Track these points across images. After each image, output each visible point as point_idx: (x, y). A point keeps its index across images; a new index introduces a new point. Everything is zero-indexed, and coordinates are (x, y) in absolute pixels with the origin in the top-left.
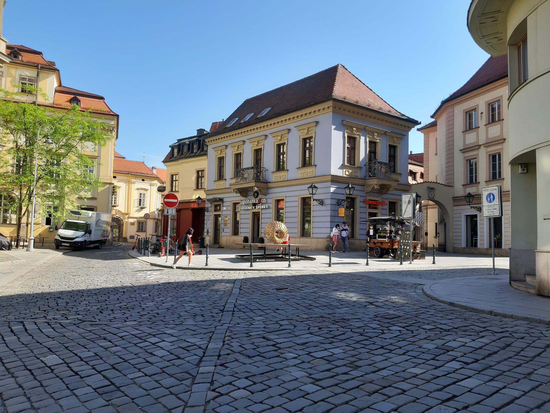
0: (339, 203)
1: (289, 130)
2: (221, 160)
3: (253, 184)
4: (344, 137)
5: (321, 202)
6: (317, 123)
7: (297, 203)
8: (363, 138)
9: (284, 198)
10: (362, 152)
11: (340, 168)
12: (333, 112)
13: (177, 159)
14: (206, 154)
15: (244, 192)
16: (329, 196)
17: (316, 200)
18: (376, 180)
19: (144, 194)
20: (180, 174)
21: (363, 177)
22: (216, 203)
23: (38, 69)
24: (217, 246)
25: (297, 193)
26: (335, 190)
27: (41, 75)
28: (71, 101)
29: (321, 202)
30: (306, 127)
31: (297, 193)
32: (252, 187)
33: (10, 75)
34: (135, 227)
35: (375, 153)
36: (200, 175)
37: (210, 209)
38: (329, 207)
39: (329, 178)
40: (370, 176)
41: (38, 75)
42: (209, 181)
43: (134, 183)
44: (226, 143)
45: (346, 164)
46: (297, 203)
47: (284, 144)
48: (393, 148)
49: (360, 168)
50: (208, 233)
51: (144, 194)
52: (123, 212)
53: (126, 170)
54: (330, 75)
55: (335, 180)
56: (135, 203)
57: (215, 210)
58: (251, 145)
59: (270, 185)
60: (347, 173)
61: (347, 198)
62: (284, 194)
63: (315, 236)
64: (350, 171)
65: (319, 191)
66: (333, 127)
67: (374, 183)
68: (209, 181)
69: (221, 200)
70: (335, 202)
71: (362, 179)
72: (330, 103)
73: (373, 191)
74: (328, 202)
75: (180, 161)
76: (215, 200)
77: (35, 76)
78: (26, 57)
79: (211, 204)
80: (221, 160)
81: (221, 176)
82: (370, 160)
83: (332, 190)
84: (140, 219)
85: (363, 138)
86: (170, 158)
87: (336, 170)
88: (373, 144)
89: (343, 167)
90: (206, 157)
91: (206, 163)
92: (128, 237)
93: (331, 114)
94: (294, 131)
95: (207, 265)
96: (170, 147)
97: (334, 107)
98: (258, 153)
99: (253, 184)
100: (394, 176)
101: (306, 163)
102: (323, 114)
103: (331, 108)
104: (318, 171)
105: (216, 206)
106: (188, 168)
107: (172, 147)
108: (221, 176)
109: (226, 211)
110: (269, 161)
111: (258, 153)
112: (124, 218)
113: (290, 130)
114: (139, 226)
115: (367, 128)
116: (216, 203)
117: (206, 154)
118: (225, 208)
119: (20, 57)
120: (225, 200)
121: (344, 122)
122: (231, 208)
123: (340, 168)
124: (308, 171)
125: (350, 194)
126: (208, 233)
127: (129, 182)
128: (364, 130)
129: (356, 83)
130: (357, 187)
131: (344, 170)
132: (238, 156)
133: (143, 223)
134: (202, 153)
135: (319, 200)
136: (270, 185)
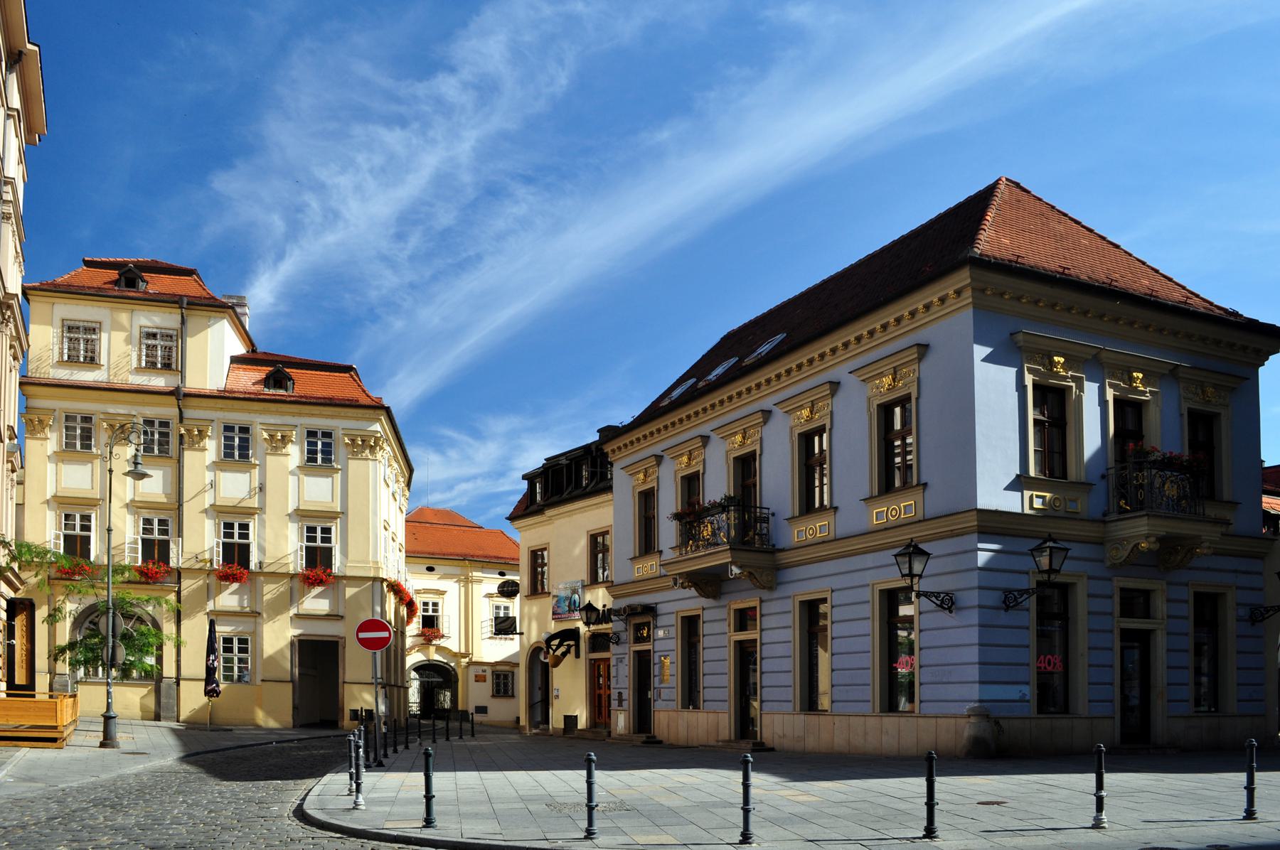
0: (1010, 600)
1: (835, 386)
2: (647, 499)
3: (726, 558)
4: (1021, 387)
5: (947, 602)
6: (923, 349)
7: (867, 608)
8: (1091, 389)
9: (828, 595)
10: (1092, 434)
11: (1013, 486)
12: (976, 306)
13: (540, 511)
14: (609, 489)
15: (709, 583)
16: (973, 580)
17: (927, 595)
18: (1145, 520)
19: (435, 604)
20: (552, 547)
21: (1099, 516)
22: (639, 620)
23: (181, 308)
24: (643, 737)
25: (868, 577)
26: (991, 560)
27: (191, 323)
28: (266, 382)
29: (947, 602)
30: (887, 367)
31: (868, 577)
32: (724, 567)
33: (118, 327)
34: (487, 687)
35: (1138, 435)
36: (598, 545)
37: (623, 636)
38: (973, 617)
39: (973, 522)
40: (1122, 511)
41: (183, 322)
42: (622, 564)
43: (480, 582)
44: (657, 450)
45: (1032, 473)
46: (867, 608)
47: (820, 431)
48: (1202, 427)
49: (1085, 486)
50: (620, 704)
51: (435, 604)
52: (456, 650)
53: (459, 551)
54: (972, 211)
55: (994, 524)
56: (484, 630)
57: (639, 639)
58: (727, 445)
59: (784, 558)
60: (1038, 504)
61: (1039, 583)
62: (835, 582)
63: (929, 708)
64: (1048, 495)
65: (933, 565)
66: (980, 351)
67: (1139, 531)
68: (622, 564)
69: (650, 610)
70: (994, 598)
71: (1093, 521)
72: (963, 278)
73: (1137, 561)
74: (972, 598)
75: (549, 513)
76: (631, 612)
77: (177, 325)
78: (157, 284)
79: (626, 621)
80: (647, 499)
81: (647, 544)
82: (1121, 456)
83: (982, 558)
84: (499, 668)
85: (1091, 389)
86: (527, 508)
87: (995, 490)
88: (1128, 414)
89: (1021, 483)
90: (609, 496)
91: (606, 513)
92: (471, 710)
93: (969, 313)
94: (851, 385)
95: (429, 822)
96: (524, 477)
97: (978, 291)
98: (746, 466)
99: (726, 558)
100: (1212, 511)
101: (891, 475)
102: (943, 312)
103: (968, 294)
104: (936, 501)
105: (638, 628)
106: (566, 532)
107: (530, 478)
108: (647, 544)
109: (666, 639)
110: (777, 482)
111: (746, 466)
112: (458, 663)
113: (844, 388)
114: (498, 685)
115: (1104, 355)
116: (639, 620)
117: (609, 489)
118: (661, 633)
119: (142, 285)
120: (662, 609)
121: (1020, 337)
122: (676, 631)
123: (1013, 486)
124: (901, 507)
125: (1051, 571)
126: (620, 704)
127: (467, 581)
128: (1096, 366)
129: (1061, 227)
130: (1076, 549)
131: (1027, 494)
132: (691, 483)
133: (506, 677)
134: (601, 485)
135: (936, 595)
136: (784, 558)
